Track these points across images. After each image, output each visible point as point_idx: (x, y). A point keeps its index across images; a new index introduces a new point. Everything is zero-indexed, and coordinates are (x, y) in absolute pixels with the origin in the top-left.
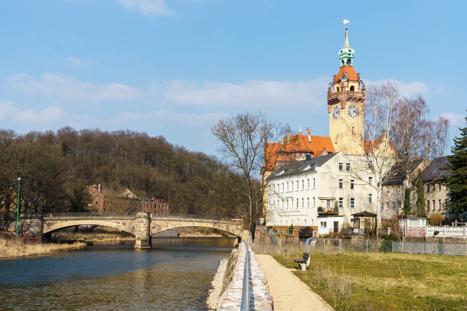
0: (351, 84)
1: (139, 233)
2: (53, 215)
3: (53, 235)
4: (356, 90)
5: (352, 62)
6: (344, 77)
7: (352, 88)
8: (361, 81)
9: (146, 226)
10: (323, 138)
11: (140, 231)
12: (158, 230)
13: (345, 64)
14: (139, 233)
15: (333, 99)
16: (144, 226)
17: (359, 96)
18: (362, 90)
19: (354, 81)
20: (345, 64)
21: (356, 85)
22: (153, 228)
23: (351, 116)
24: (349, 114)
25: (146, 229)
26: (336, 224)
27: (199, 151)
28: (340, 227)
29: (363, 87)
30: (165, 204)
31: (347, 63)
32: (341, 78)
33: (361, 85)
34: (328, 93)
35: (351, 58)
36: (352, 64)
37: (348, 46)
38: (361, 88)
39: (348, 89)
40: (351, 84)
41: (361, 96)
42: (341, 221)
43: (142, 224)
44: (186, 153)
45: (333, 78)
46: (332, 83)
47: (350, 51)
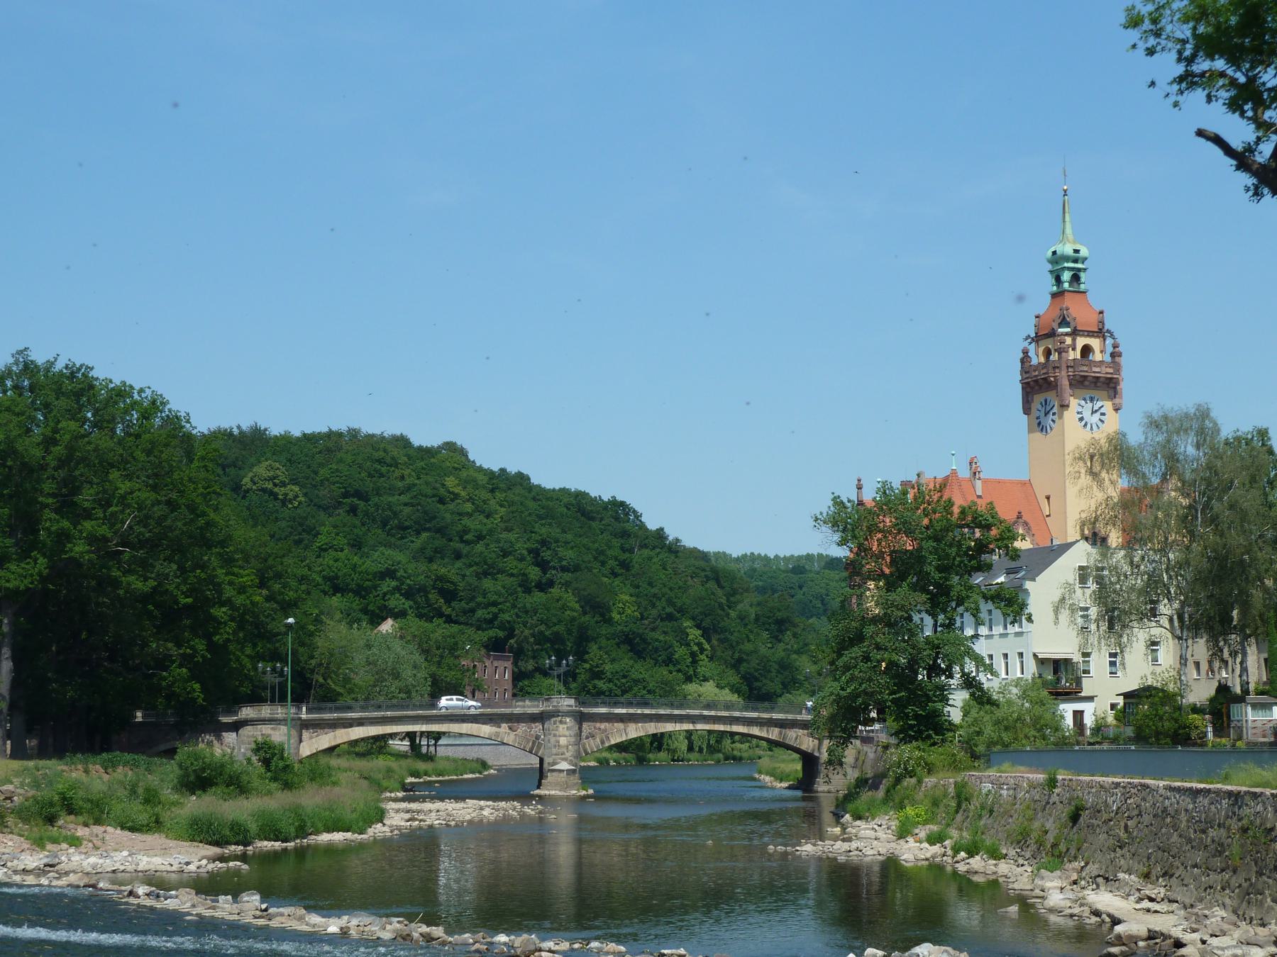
0: (1081, 342)
1: (554, 751)
2: (309, 711)
3: (727, 742)
4: (1097, 356)
5: (1083, 280)
6: (1064, 322)
7: (1086, 350)
8: (1108, 331)
9: (572, 733)
10: (1012, 482)
11: (558, 745)
12: (603, 742)
13: (1066, 285)
14: (554, 751)
15: (1036, 381)
16: (567, 733)
17: (1104, 372)
18: (1113, 355)
19: (1090, 334)
20: (1066, 285)
21: (1095, 343)
22: (587, 738)
23: (1086, 425)
24: (1081, 419)
25: (573, 740)
26: (1078, 715)
27: (574, 485)
28: (1089, 721)
29: (1115, 346)
30: (501, 664)
31: (1071, 283)
32: (1055, 325)
33: (1109, 341)
34: (1022, 361)
35: (1079, 270)
36: (1082, 286)
37: (1071, 237)
38: (1109, 349)
39: (1074, 355)
40: (1081, 342)
41: (1111, 371)
42: (1089, 709)
43: (561, 726)
44: (544, 490)
45: (1034, 321)
46: (1033, 335)
47: (1077, 251)
